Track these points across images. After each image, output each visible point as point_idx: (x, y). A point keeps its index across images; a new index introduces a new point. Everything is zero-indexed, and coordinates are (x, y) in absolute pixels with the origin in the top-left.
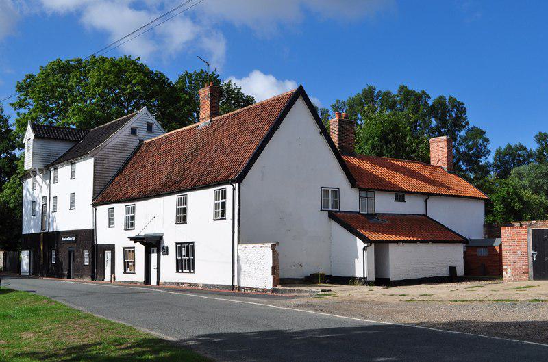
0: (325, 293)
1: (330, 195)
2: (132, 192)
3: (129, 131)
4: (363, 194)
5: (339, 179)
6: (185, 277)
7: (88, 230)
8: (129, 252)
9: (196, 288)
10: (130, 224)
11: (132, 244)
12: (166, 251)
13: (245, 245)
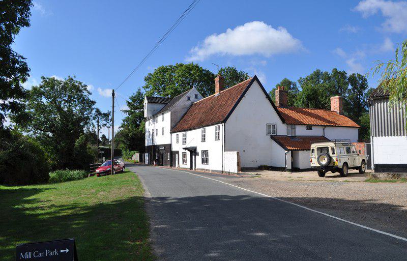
1: (271, 127)
2: (185, 127)
4: (289, 126)
5: (276, 120)
6: (205, 167)
8: (184, 155)
10: (184, 142)
11: (184, 151)
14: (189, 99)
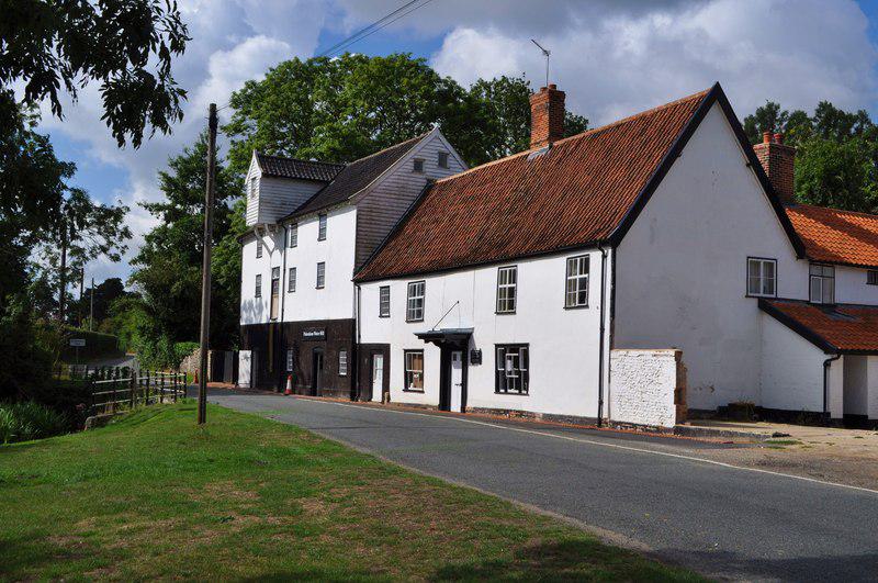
0: (782, 439)
1: (761, 270)
2: (422, 261)
3: (410, 166)
4: (816, 270)
5: (776, 245)
6: (510, 401)
7: (345, 320)
8: (414, 358)
9: (531, 419)
10: (416, 312)
11: (420, 344)
12: (477, 358)
13: (623, 352)
14: (418, 165)
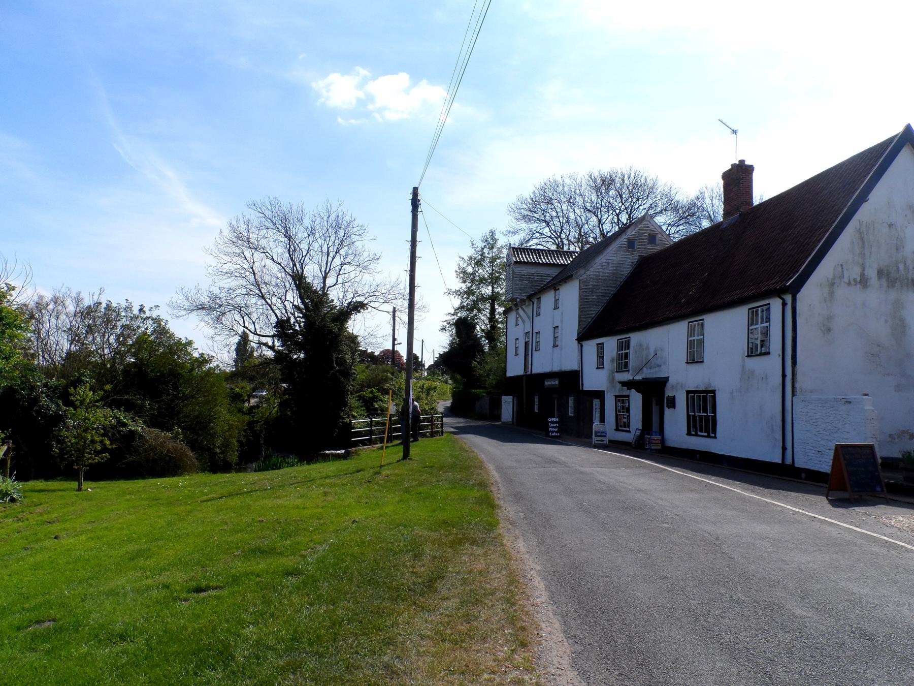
8: (621, 399)
